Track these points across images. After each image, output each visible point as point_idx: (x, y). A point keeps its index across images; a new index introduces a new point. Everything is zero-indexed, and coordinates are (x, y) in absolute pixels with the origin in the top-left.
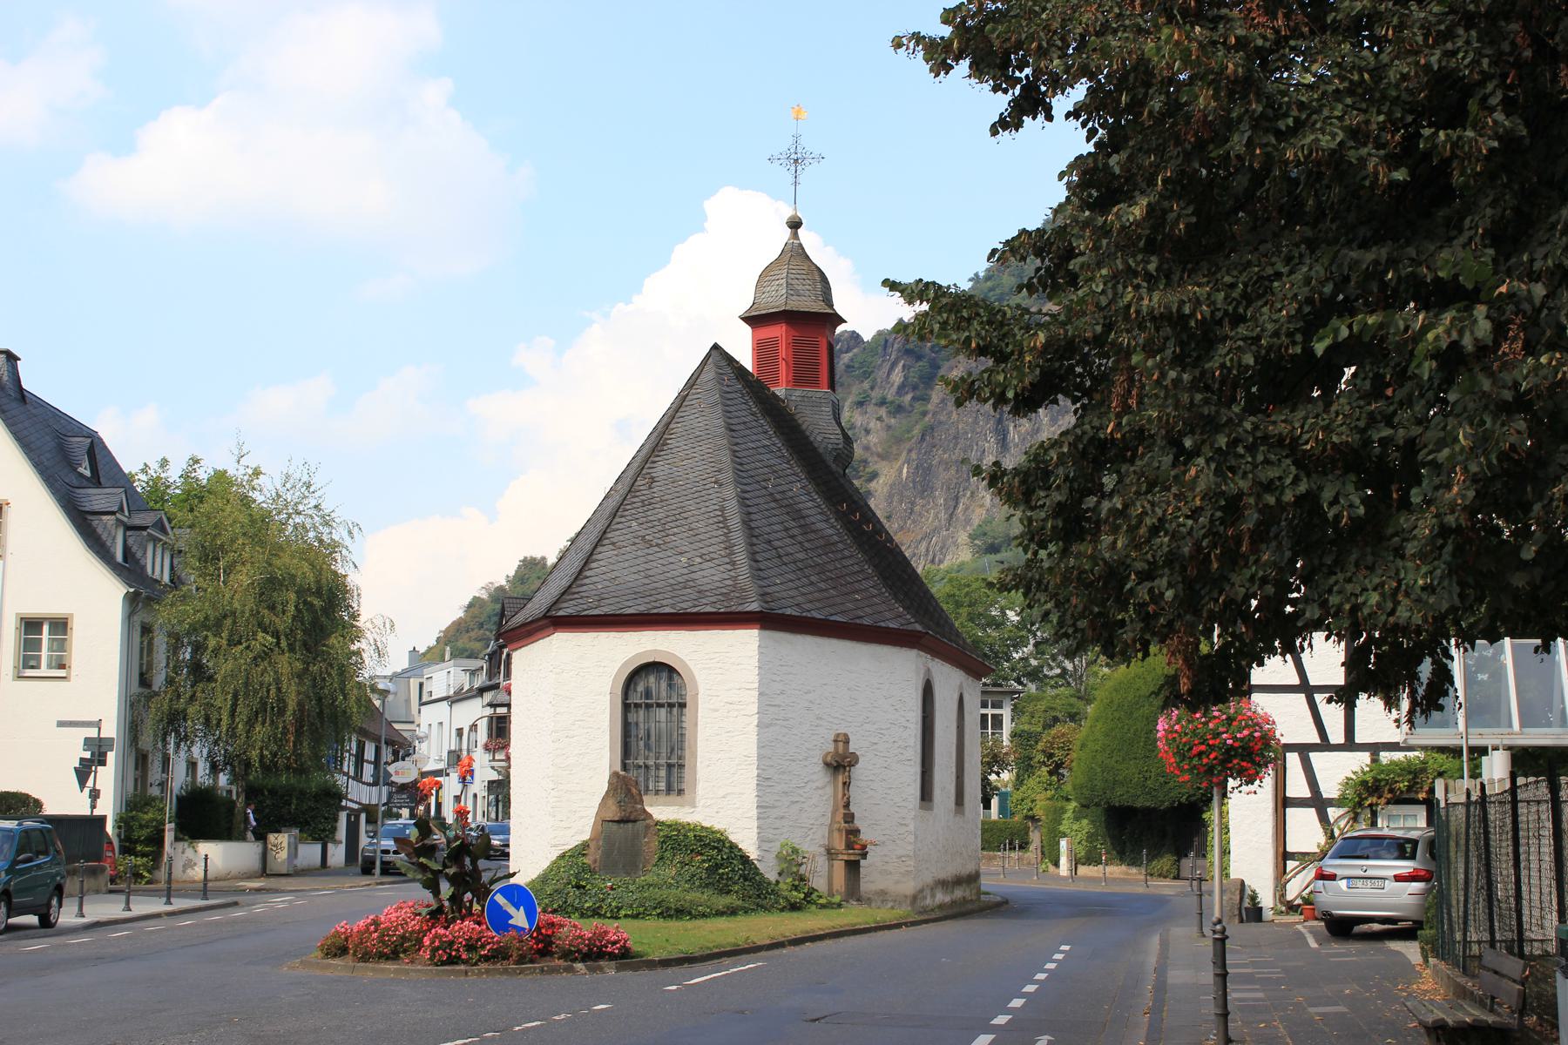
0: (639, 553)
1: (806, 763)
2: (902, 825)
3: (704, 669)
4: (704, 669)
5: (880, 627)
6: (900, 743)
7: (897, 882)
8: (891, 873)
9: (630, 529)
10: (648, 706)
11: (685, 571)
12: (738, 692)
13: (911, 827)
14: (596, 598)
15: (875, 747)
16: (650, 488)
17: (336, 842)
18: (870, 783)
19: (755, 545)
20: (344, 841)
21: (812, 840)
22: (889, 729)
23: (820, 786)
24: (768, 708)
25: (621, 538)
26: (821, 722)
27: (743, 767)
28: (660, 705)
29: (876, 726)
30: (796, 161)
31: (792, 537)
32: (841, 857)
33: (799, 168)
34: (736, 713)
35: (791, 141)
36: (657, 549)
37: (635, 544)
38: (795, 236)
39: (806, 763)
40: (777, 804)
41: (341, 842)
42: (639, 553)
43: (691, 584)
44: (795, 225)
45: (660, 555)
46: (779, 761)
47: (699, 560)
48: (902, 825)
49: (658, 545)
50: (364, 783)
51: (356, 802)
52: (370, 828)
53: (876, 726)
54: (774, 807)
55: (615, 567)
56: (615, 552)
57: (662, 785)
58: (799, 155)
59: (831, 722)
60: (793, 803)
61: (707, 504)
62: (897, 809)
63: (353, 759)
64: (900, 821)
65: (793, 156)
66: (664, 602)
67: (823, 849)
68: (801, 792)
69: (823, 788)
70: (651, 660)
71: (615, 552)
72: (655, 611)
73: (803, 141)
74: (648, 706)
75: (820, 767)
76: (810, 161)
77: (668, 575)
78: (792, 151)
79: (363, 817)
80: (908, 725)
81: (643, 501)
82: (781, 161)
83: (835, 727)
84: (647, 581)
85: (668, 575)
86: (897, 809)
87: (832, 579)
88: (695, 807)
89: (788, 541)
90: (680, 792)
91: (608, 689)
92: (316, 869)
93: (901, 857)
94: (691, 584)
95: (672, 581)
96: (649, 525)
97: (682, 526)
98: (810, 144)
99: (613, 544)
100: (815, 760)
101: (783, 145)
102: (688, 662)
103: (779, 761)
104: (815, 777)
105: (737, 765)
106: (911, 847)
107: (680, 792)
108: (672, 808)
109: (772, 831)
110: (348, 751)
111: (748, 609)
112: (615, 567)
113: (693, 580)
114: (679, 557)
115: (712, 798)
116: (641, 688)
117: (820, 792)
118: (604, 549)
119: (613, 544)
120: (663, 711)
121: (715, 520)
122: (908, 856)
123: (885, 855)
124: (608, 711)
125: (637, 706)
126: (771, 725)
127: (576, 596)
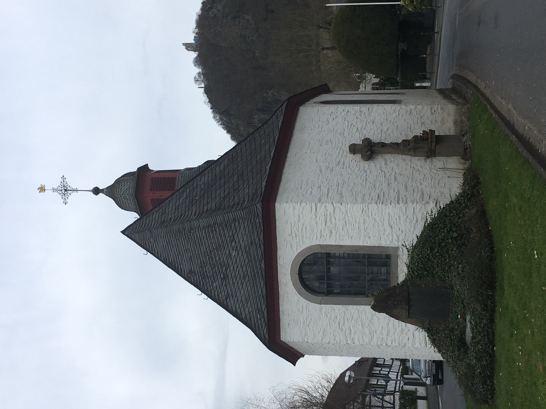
0: (231, 282)
1: (368, 172)
2: (411, 113)
3: (303, 240)
4: (303, 240)
5: (281, 127)
6: (358, 114)
7: (449, 115)
8: (443, 118)
9: (218, 287)
10: (329, 278)
11: (240, 253)
12: (318, 217)
13: (412, 107)
14: (257, 312)
15: (359, 129)
16: (195, 273)
17: (416, 392)
18: (383, 132)
19: (225, 206)
20: (416, 387)
21: (421, 167)
22: (348, 122)
23: (384, 163)
24: (329, 196)
25: (223, 293)
26: (342, 162)
27: (370, 214)
28: (328, 270)
29: (346, 129)
30: (66, 190)
31: (225, 183)
32: (433, 147)
33: (69, 189)
34: (333, 218)
35: (56, 193)
36: (228, 270)
37: (226, 285)
38: (102, 191)
39: (368, 172)
40: (396, 190)
41: (416, 388)
42: (231, 282)
43: (247, 248)
44: (96, 191)
45: (232, 268)
46: (367, 189)
47: (233, 243)
48: (411, 113)
49: (226, 270)
50: (392, 364)
51: (400, 368)
52: (410, 373)
53: (346, 129)
54: (399, 191)
55: (240, 298)
56: (231, 298)
57: (384, 270)
58: (63, 189)
59: (342, 156)
60: (395, 179)
61: (202, 238)
62: (401, 115)
63: (383, 369)
64: (408, 114)
65: (63, 192)
66: (259, 267)
67: (428, 160)
68: (388, 175)
69: (386, 161)
70: (297, 276)
71: (231, 298)
72: (264, 273)
73: (55, 187)
74: (329, 278)
75: (371, 163)
76: (65, 183)
77: (243, 264)
78: (61, 192)
79: (405, 376)
80: (346, 110)
81: (202, 279)
82: (66, 198)
83: (345, 154)
84: (247, 278)
85: (243, 264)
86: (401, 115)
87: (251, 158)
88: (398, 247)
89: (226, 186)
90: (388, 257)
91: (317, 306)
92: (428, 401)
93: (432, 113)
94: (247, 248)
95: (246, 261)
96: (215, 275)
97: (214, 254)
98: (57, 184)
99: (226, 299)
100: (367, 166)
101: (57, 196)
102: (299, 252)
103: (367, 189)
104: (378, 166)
105: (369, 217)
106: (426, 107)
107: (388, 257)
108: (399, 263)
109: (415, 193)
110: (380, 371)
111: (261, 210)
112: (240, 298)
113: (245, 247)
114: (233, 256)
115: (392, 236)
116: (317, 284)
117: (388, 162)
118: (229, 304)
119: (226, 299)
120: (332, 269)
121: (210, 233)
122: (431, 108)
123: (431, 122)
124: (332, 306)
125: (329, 286)
126: (341, 194)
127: (257, 325)
